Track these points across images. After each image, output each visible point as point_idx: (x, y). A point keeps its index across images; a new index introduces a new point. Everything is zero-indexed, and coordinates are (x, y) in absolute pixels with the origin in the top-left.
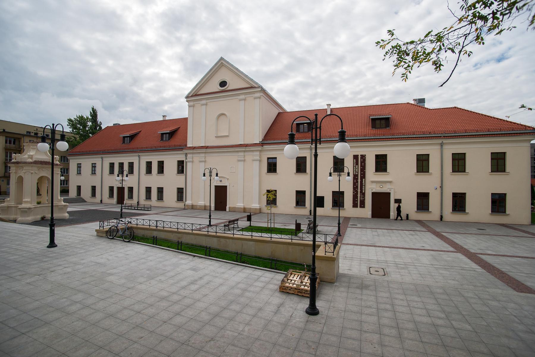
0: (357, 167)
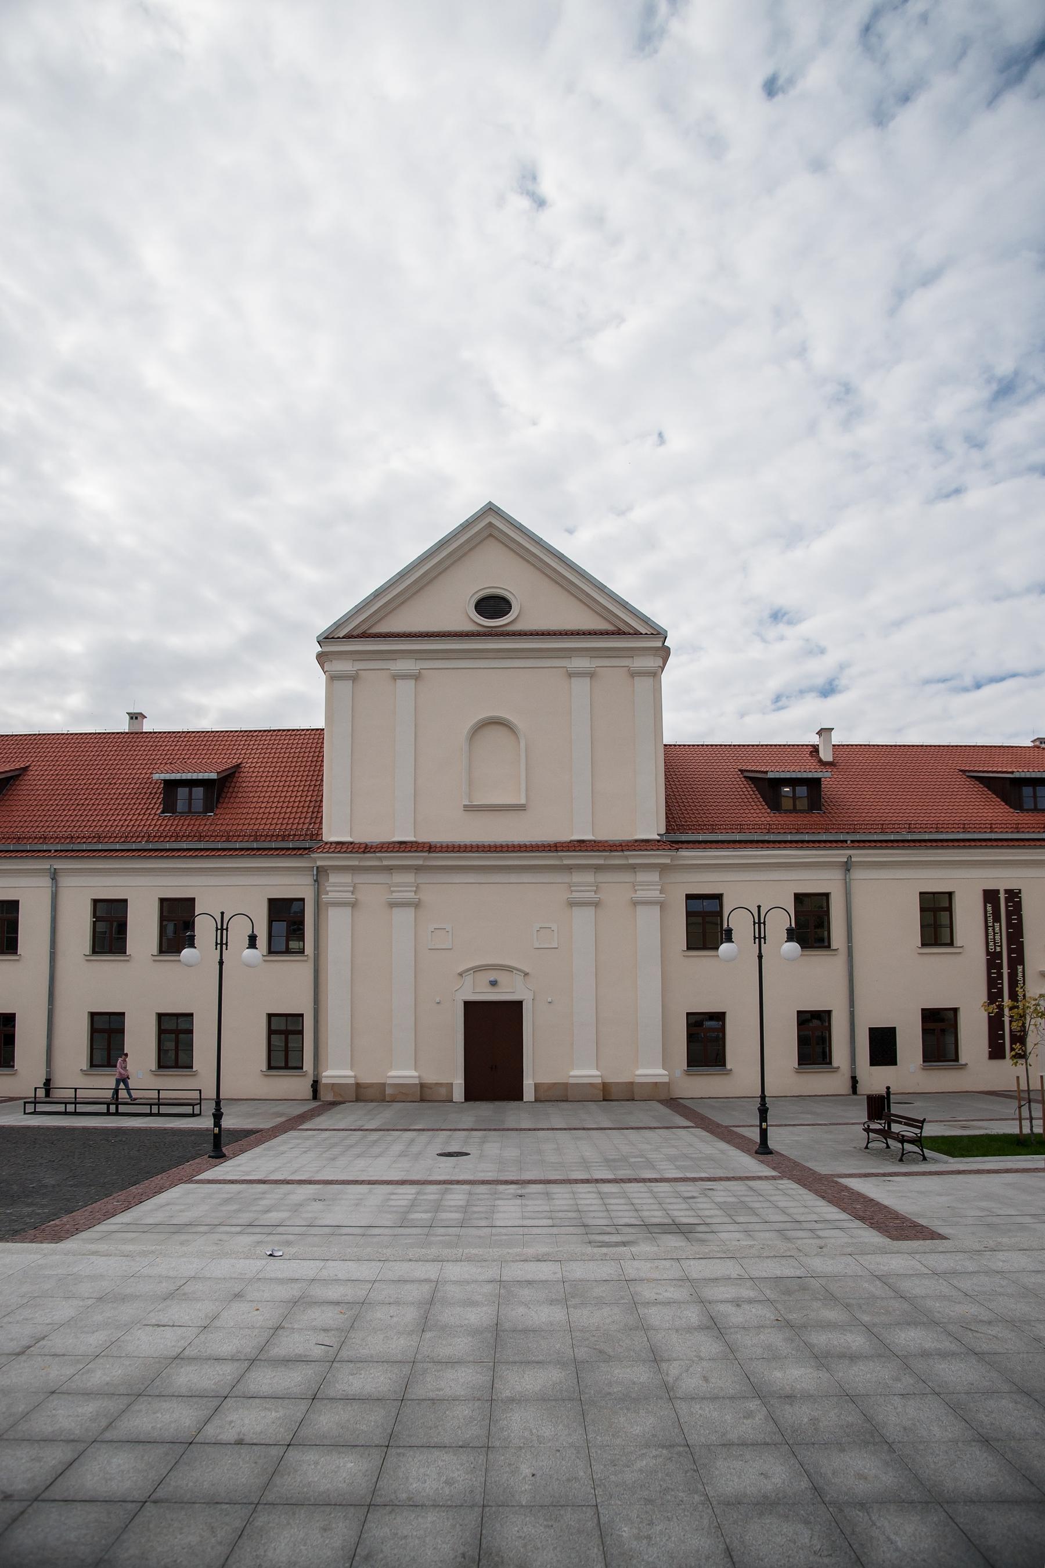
0: (997, 929)
